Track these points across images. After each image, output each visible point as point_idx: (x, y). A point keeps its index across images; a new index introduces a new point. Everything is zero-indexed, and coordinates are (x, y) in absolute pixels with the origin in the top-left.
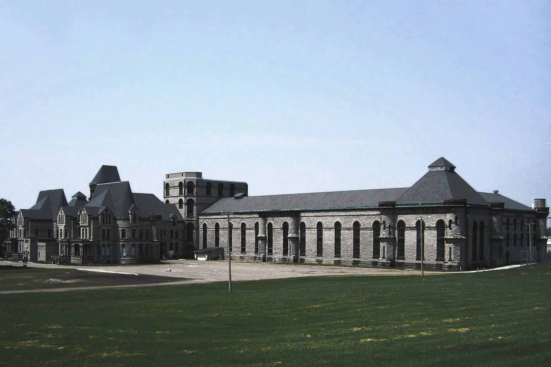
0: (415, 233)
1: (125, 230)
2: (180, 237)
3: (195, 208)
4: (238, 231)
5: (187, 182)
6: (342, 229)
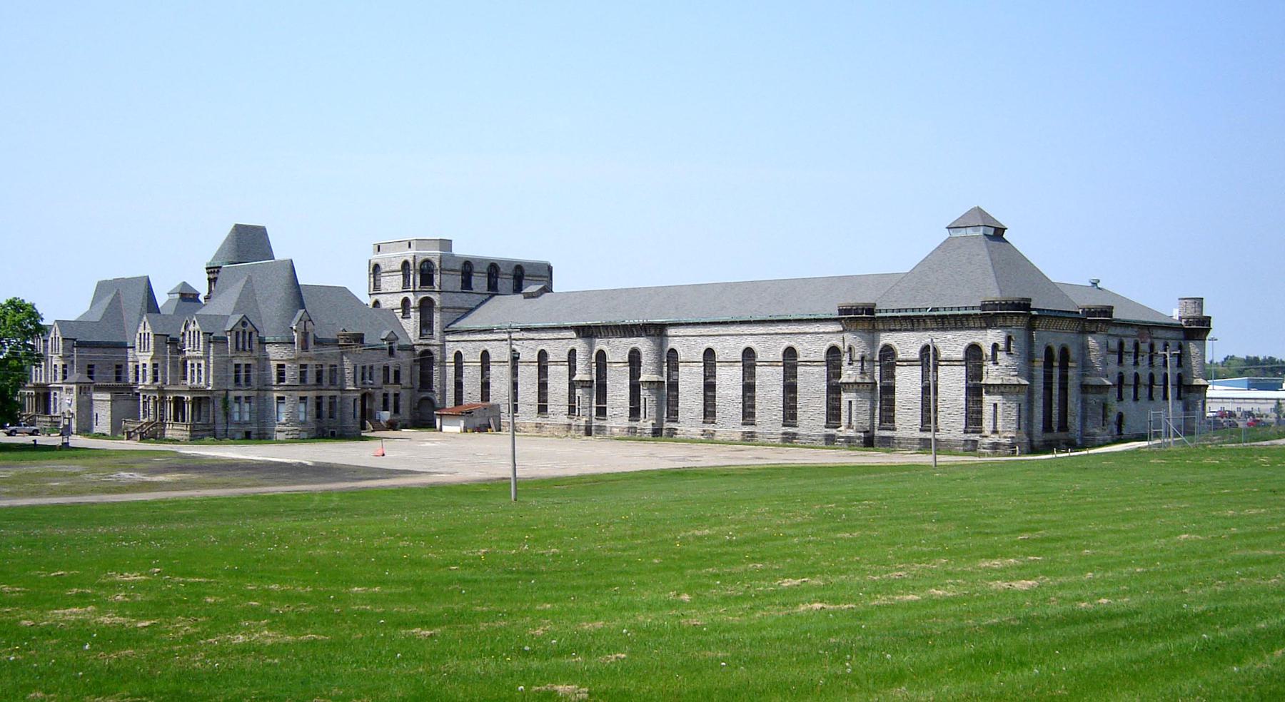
1: (283, 366)
2: (405, 380)
3: (437, 317)
4: (531, 367)
5: (419, 260)
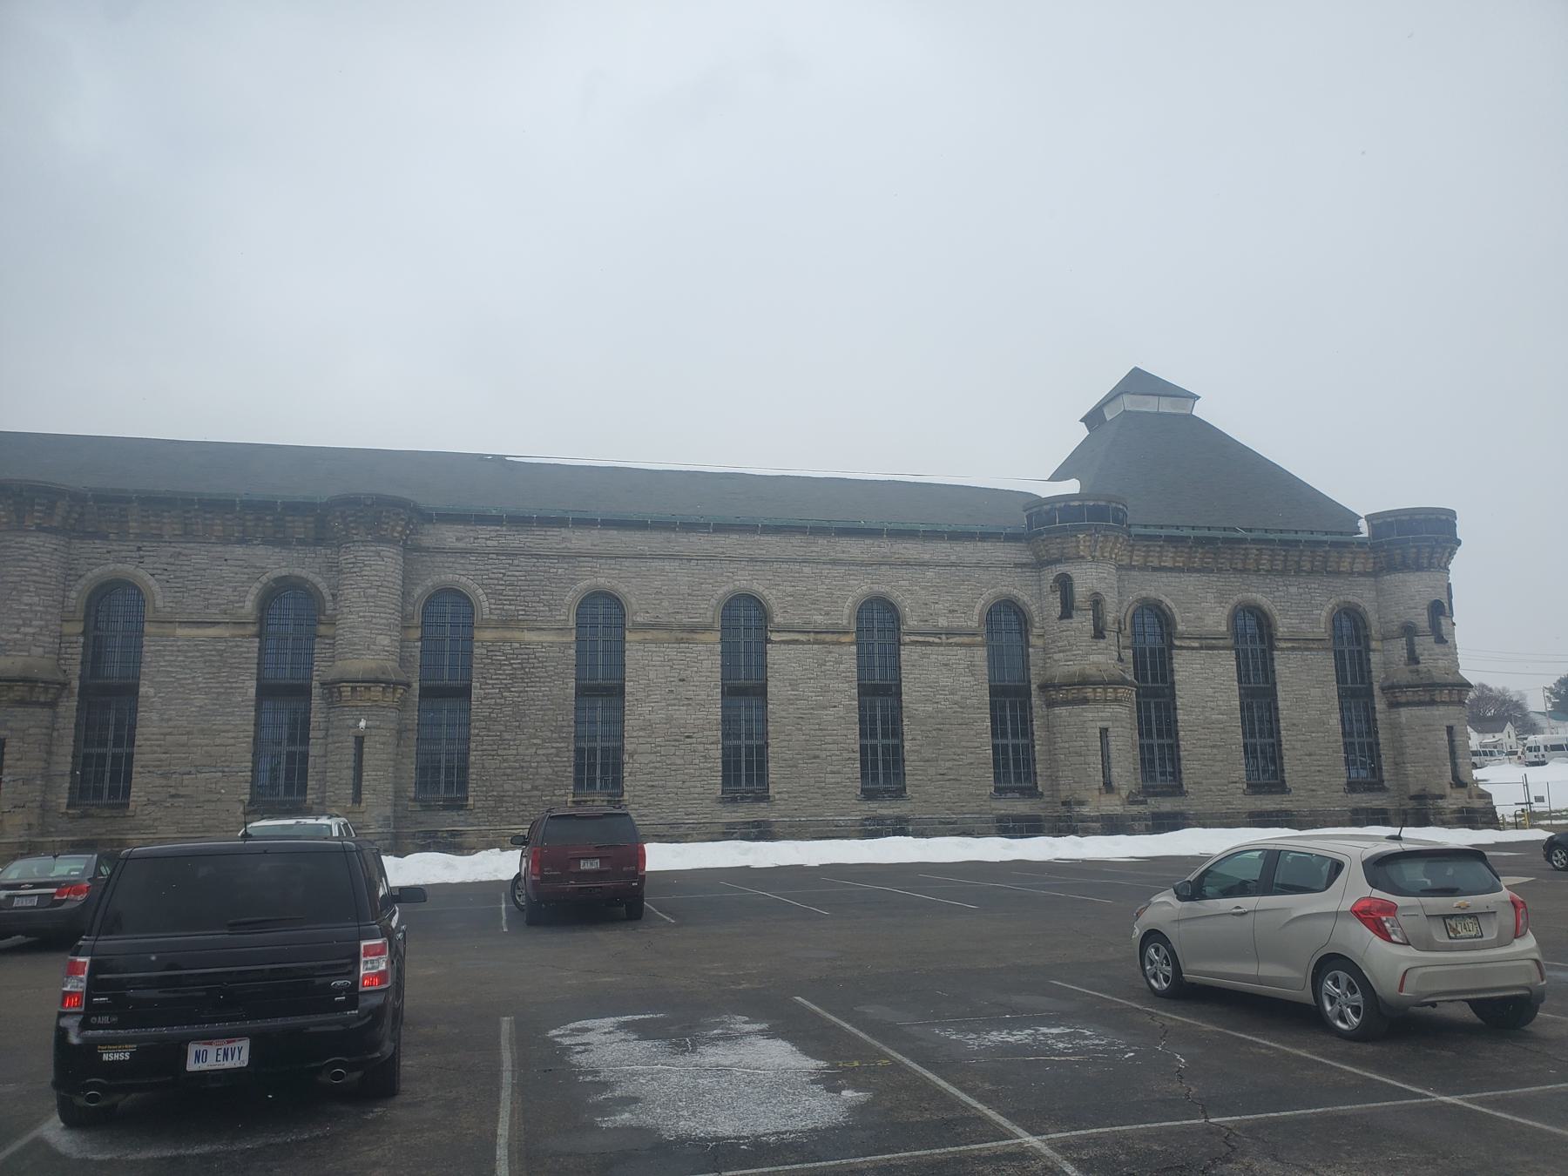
0: (1226, 664)
6: (907, 639)
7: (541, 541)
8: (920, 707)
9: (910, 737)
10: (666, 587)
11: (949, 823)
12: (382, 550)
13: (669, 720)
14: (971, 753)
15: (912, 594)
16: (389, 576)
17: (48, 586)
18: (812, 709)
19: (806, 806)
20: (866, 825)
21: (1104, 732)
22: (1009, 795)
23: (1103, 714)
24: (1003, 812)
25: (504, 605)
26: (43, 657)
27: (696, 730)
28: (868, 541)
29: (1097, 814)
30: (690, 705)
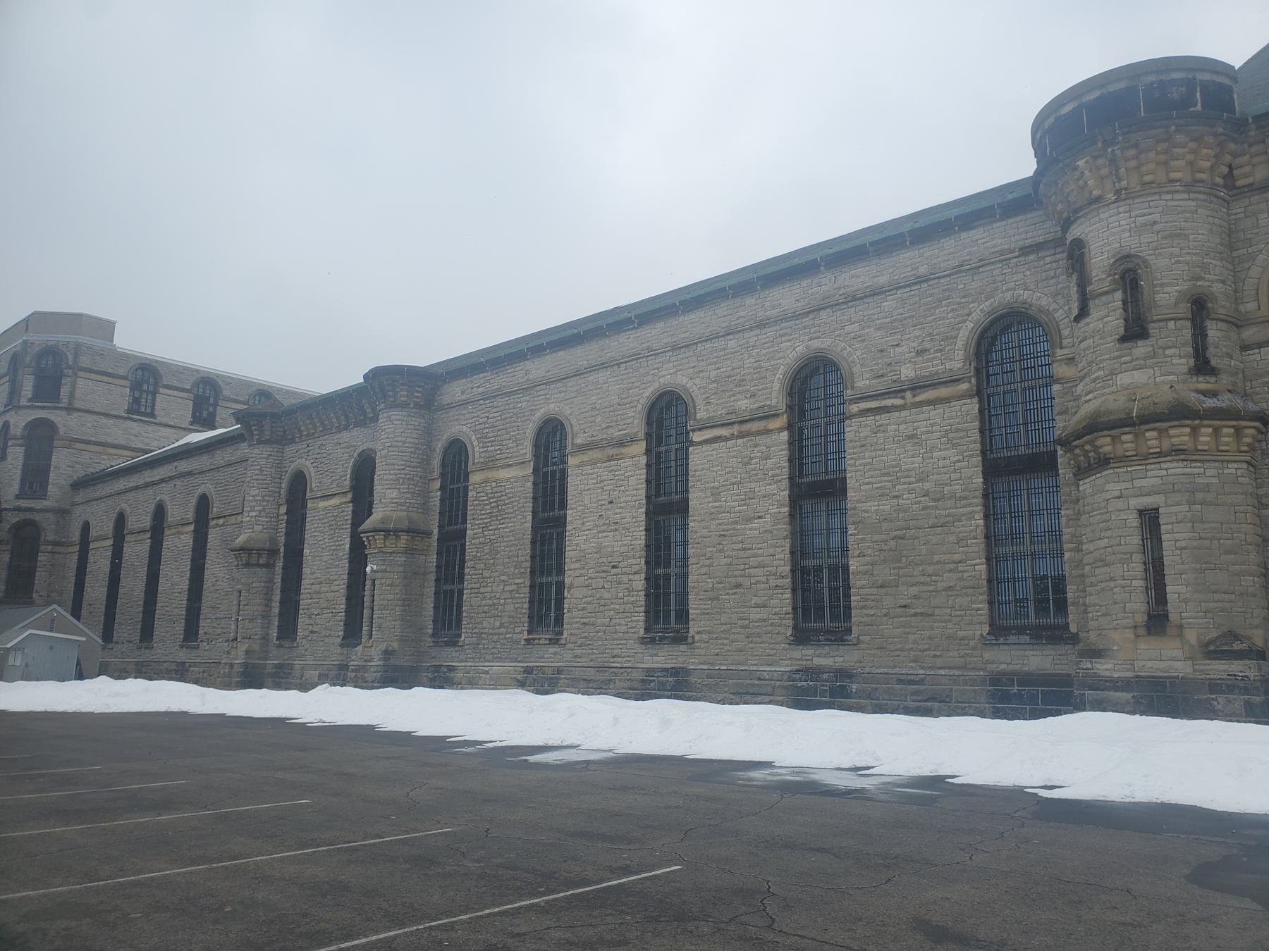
7: (511, 379)
8: (872, 506)
9: (857, 553)
10: (600, 401)
11: (911, 682)
12: (391, 415)
13: (599, 549)
14: (950, 571)
15: (863, 341)
16: (398, 436)
17: (265, 482)
18: (736, 523)
19: (728, 651)
20: (794, 680)
21: (1150, 520)
22: (1012, 639)
23: (1143, 483)
24: (1003, 667)
25: (488, 447)
26: (262, 532)
27: (621, 559)
28: (805, 283)
29: (1130, 674)
30: (616, 530)
